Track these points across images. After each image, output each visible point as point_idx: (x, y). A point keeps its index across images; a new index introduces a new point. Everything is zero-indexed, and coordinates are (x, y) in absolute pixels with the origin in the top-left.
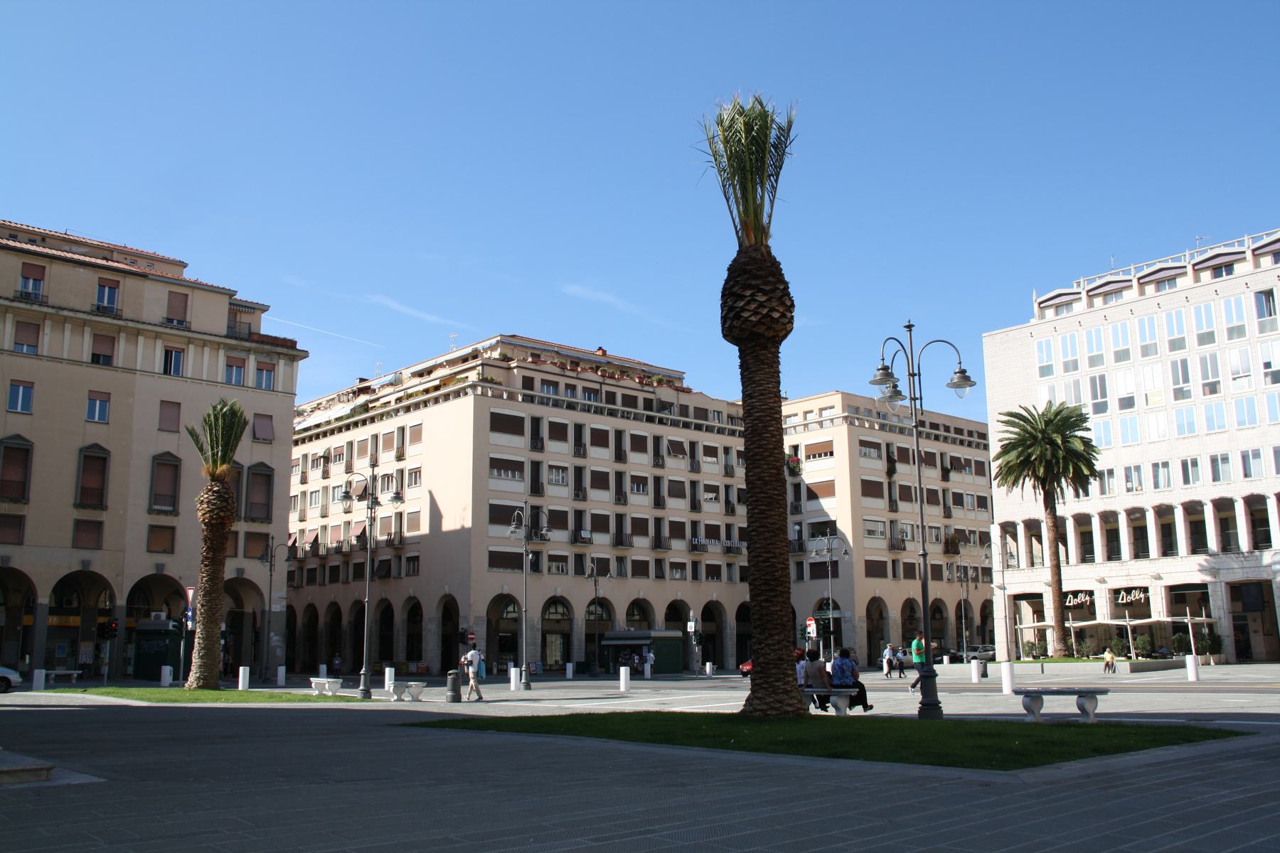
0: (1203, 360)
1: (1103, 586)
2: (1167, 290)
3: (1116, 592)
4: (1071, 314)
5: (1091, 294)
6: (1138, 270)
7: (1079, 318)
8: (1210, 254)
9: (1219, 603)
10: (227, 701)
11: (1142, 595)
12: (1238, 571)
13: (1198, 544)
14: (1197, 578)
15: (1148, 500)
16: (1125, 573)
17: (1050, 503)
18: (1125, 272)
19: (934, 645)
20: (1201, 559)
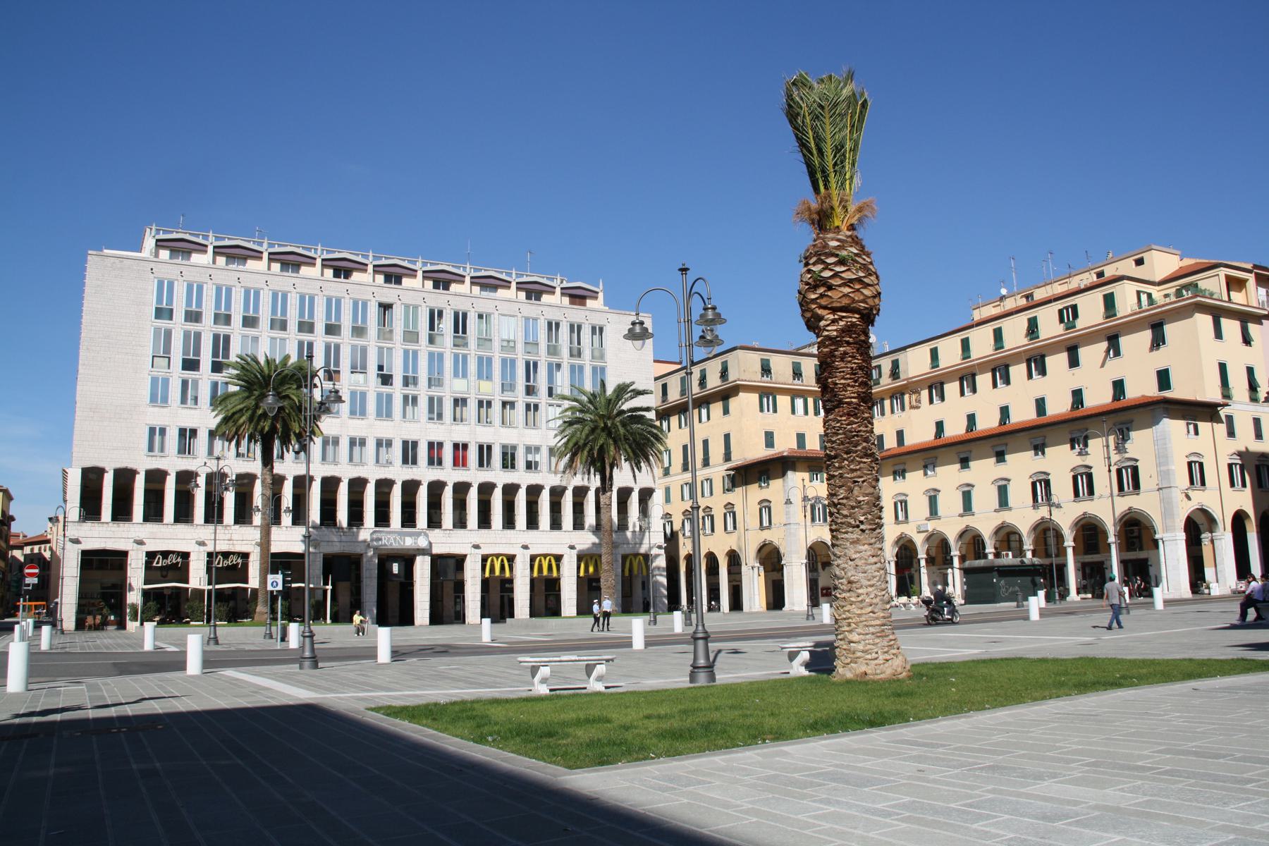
0: (328, 348)
1: (202, 548)
2: (179, 261)
3: (151, 555)
4: (184, 262)
5: (160, 244)
6: (271, 245)
7: (497, 303)
8: (483, 273)
9: (314, 568)
10: (456, 681)
11: (240, 561)
12: (335, 544)
13: (299, 516)
14: (299, 548)
15: (346, 472)
16: (228, 537)
17: (267, 460)
18: (206, 237)
19: (940, 587)
20: (301, 530)
